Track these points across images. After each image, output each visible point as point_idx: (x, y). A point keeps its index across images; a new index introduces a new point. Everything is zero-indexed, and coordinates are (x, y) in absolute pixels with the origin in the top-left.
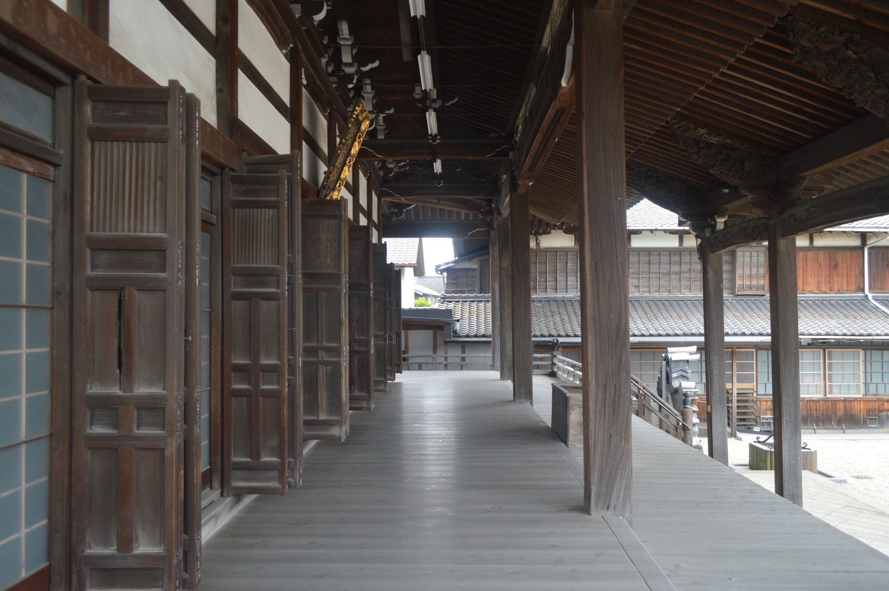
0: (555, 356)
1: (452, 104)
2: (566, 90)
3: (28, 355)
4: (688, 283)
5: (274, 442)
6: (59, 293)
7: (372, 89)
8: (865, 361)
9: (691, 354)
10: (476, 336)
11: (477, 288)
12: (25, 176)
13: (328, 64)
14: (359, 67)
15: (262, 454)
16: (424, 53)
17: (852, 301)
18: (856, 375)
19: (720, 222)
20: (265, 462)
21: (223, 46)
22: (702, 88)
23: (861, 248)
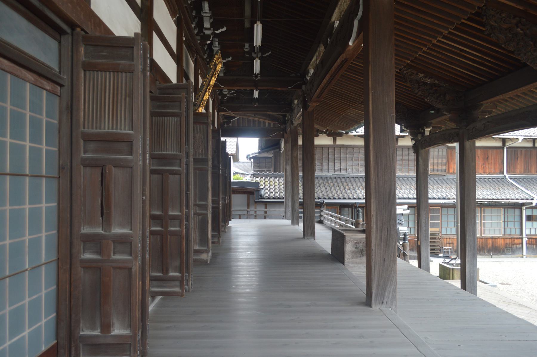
0: (322, 211)
1: (267, 56)
2: (351, 48)
3: (29, 209)
4: (401, 167)
5: (177, 263)
6: (63, 168)
7: (219, 44)
8: (504, 215)
9: (404, 210)
10: (274, 198)
11: (273, 169)
12: (45, 92)
13: (195, 28)
14: (214, 30)
15: (170, 271)
16: (258, 23)
17: (497, 179)
18: (499, 223)
19: (427, 131)
20: (171, 276)
21: (144, 12)
22: (425, 49)
23: (503, 148)
